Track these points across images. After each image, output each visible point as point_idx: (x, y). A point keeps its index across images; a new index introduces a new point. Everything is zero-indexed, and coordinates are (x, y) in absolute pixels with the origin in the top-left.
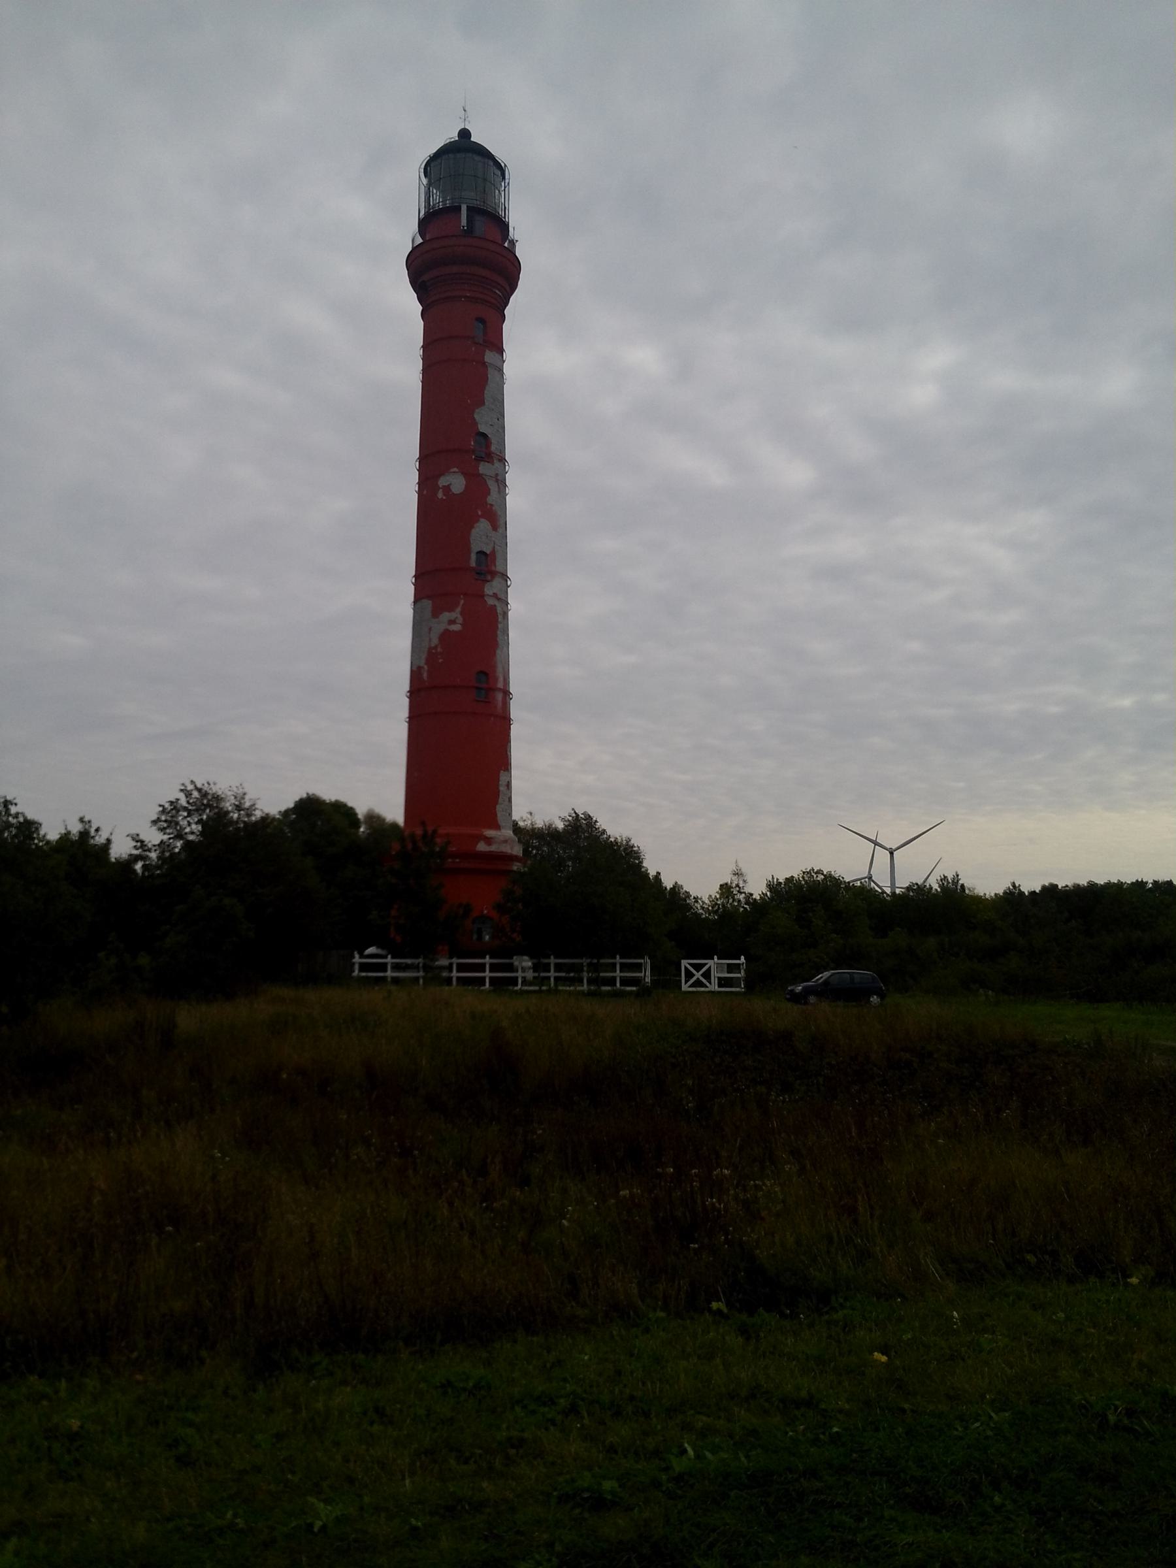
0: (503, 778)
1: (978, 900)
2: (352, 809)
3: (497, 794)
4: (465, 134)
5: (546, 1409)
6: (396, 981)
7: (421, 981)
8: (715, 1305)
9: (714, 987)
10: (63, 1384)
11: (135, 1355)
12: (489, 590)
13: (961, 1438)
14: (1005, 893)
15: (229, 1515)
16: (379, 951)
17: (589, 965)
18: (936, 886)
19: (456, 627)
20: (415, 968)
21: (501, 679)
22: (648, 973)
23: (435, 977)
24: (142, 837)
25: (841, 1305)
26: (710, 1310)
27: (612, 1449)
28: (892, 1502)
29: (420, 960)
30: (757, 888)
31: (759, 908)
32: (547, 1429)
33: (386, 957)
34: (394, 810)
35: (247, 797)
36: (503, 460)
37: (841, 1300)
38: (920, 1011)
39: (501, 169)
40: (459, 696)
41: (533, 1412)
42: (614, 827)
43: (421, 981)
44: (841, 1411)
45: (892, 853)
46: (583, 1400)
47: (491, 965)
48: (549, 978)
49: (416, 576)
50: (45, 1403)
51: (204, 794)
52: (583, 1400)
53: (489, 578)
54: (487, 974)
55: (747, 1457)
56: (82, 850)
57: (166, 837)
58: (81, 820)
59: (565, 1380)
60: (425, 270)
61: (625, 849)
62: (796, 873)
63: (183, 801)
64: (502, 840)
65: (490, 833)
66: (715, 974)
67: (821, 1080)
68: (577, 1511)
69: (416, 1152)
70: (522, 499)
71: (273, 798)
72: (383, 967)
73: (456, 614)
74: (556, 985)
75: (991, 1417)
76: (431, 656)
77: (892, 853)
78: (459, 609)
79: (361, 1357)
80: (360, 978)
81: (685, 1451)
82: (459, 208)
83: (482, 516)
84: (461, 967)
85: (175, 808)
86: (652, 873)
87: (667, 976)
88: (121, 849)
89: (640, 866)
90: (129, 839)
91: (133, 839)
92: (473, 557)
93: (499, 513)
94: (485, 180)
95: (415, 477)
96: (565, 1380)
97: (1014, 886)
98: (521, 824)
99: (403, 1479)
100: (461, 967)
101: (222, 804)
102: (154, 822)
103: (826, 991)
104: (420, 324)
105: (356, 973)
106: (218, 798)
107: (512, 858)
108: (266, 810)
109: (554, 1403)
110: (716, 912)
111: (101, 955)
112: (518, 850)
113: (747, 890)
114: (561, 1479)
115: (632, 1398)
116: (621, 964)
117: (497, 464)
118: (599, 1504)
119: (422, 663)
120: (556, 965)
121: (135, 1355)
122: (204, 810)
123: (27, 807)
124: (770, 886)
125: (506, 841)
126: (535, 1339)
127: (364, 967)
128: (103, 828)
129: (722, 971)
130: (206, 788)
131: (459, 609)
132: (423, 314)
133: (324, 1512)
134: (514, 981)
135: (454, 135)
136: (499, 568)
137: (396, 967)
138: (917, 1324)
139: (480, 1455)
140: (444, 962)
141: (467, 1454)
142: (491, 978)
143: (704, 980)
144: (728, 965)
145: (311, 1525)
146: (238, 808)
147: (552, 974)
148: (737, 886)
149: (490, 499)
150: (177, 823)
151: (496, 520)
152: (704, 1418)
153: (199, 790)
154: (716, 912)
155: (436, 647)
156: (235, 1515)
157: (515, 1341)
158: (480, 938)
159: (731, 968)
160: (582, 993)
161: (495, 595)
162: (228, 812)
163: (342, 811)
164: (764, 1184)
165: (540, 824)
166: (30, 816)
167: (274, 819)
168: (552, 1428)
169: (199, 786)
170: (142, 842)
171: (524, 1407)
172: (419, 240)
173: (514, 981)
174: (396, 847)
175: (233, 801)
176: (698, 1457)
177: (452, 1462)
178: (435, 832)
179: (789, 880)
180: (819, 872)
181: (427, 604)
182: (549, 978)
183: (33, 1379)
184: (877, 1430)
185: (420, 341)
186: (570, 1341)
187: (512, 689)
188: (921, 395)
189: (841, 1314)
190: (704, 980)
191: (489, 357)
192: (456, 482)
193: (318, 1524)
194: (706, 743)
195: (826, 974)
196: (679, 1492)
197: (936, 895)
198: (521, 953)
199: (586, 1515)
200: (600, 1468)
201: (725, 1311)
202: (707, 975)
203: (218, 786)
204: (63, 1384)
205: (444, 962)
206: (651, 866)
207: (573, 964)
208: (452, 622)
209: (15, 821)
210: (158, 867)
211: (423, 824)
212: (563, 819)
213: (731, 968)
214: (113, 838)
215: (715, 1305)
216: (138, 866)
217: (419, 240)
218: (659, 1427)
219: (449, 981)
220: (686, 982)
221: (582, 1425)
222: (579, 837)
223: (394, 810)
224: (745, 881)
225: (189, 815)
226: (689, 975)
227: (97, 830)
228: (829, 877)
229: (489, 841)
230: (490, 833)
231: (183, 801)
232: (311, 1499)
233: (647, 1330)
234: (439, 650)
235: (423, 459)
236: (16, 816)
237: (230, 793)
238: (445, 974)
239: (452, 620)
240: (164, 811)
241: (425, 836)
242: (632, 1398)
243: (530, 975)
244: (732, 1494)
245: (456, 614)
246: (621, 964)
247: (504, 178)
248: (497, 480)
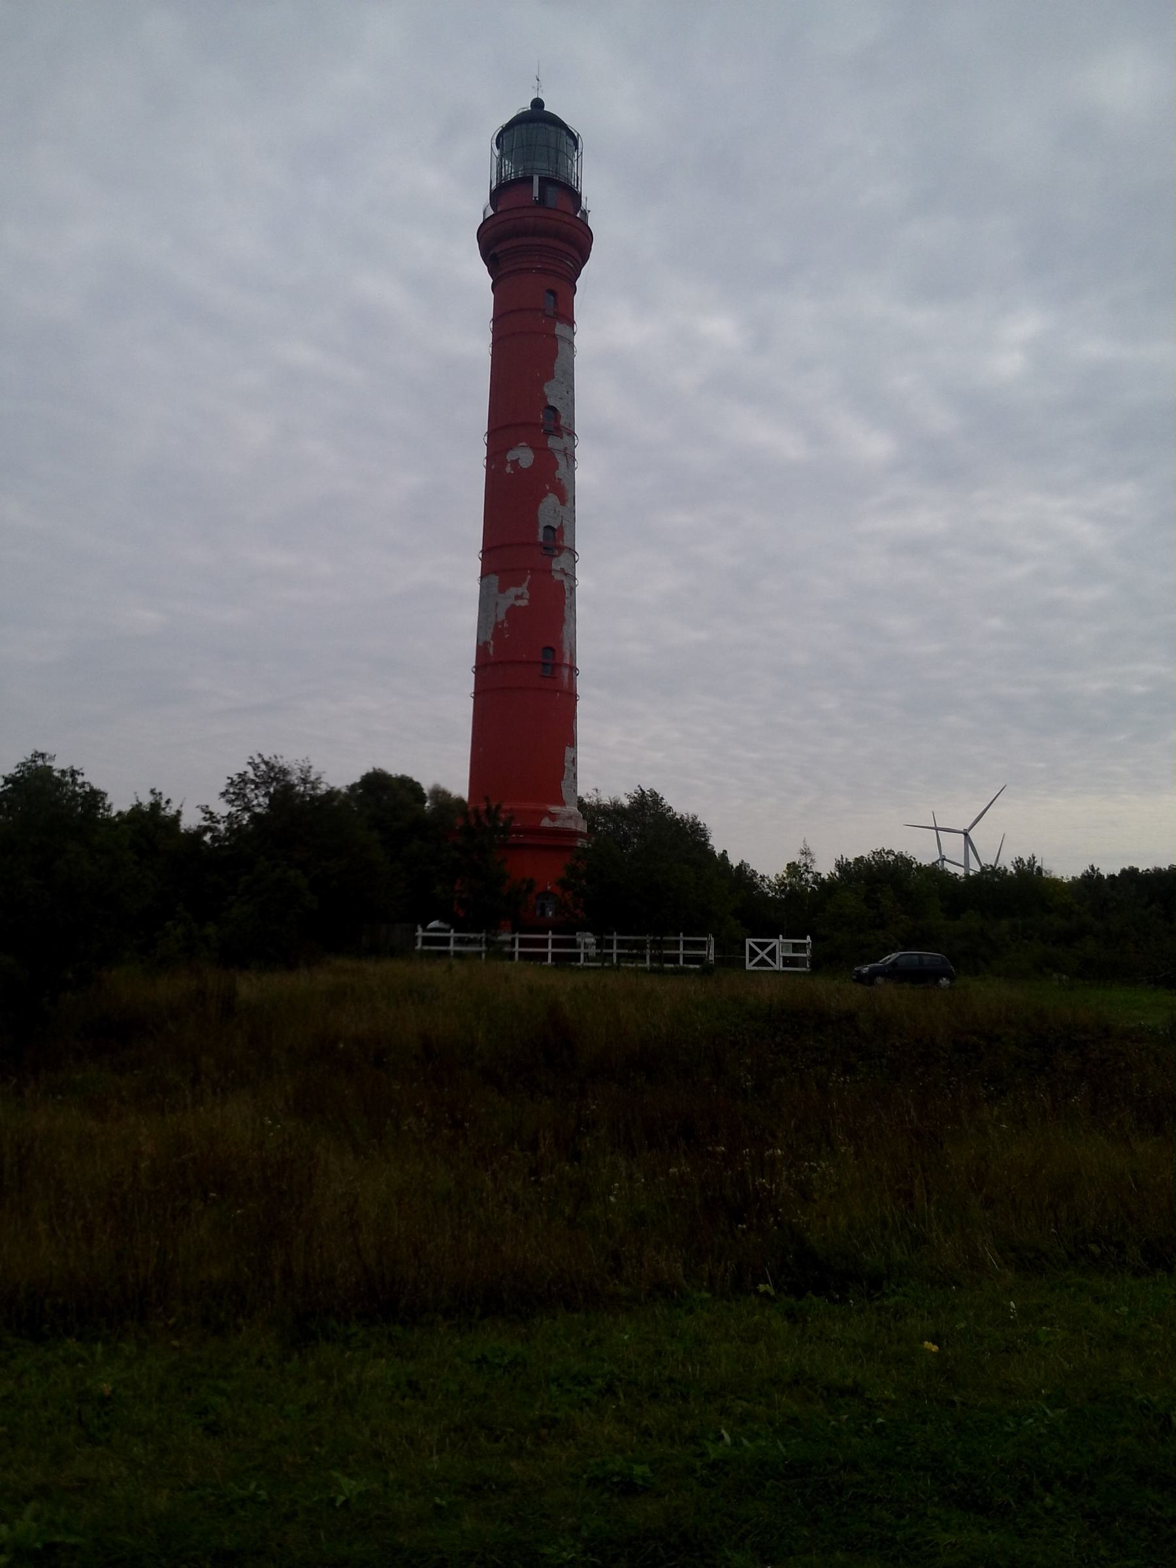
1: (1056, 883)
2: (418, 783)
3: (562, 769)
4: (538, 104)
5: (583, 1389)
6: (458, 955)
7: (483, 955)
8: (762, 1287)
9: (779, 966)
10: (99, 1347)
11: (172, 1321)
12: (556, 565)
13: (1013, 1434)
14: (1083, 876)
15: (252, 1486)
16: (442, 925)
17: (653, 942)
18: (1011, 869)
19: (523, 603)
20: (478, 942)
21: (568, 655)
22: (712, 951)
23: (498, 952)
24: (211, 809)
25: (893, 1291)
26: (757, 1292)
27: (646, 1432)
28: (936, 1499)
29: (483, 935)
30: (825, 868)
31: (827, 887)
32: (581, 1409)
33: (449, 931)
34: (459, 786)
35: (313, 770)
36: (572, 434)
37: (893, 1286)
38: (988, 994)
39: (574, 139)
40: (525, 671)
41: (569, 1391)
42: (680, 804)
43: (483, 955)
44: (887, 1401)
45: (966, 835)
46: (620, 1380)
48: (611, 954)
49: (482, 551)
50: (80, 1365)
52: (620, 1380)
53: (556, 552)
55: (785, 1445)
56: (151, 823)
57: (234, 809)
58: (152, 792)
59: (603, 1360)
60: (498, 242)
61: (691, 827)
62: (865, 852)
63: (251, 775)
64: (567, 817)
66: (780, 954)
67: (884, 1061)
68: (606, 1495)
69: (467, 1125)
70: (590, 473)
71: (339, 773)
72: (446, 941)
73: (523, 590)
74: (618, 961)
75: (1045, 1414)
76: (498, 632)
77: (966, 835)
78: (525, 585)
79: (398, 1329)
80: (422, 952)
81: (721, 1437)
82: (531, 180)
84: (524, 943)
85: (243, 780)
86: (718, 851)
87: (731, 954)
88: (191, 820)
89: (705, 844)
90: (199, 810)
91: (203, 811)
92: (541, 531)
93: (565, 482)
94: (558, 151)
95: (484, 452)
96: (603, 1360)
97: (1093, 869)
98: (587, 800)
99: (431, 1455)
100: (524, 943)
101: (288, 778)
102: (223, 794)
103: (895, 973)
105: (419, 947)
106: (284, 772)
107: (575, 834)
108: (332, 785)
109: (590, 1383)
110: (783, 892)
111: (169, 924)
112: (582, 826)
113: (815, 869)
114: (592, 1461)
115: (671, 1380)
116: (685, 942)
117: (566, 438)
118: (629, 1488)
119: (489, 637)
120: (619, 941)
121: (172, 1321)
122: (271, 783)
123: (94, 777)
124: (839, 866)
125: (570, 817)
126: (576, 1316)
127: (427, 941)
128: (173, 799)
129: (787, 951)
130: (273, 761)
131: (525, 585)
132: (494, 287)
133: (349, 1487)
134: (576, 957)
135: (527, 105)
136: (566, 543)
137: (459, 941)
138: (971, 1314)
139: (512, 1434)
140: (506, 937)
141: (498, 1432)
142: (553, 954)
143: (769, 960)
144: (794, 945)
145: (333, 1500)
146: (304, 781)
147: (615, 950)
148: (805, 865)
149: (560, 473)
150: (245, 796)
151: (564, 494)
152: (745, 1404)
153: (267, 763)
154: (783, 892)
155: (503, 622)
156: (258, 1487)
157: (555, 1318)
158: (543, 913)
159: (796, 948)
160: (644, 970)
161: (562, 570)
162: (294, 786)
163: (408, 786)
164: (819, 1166)
165: (606, 800)
166: (96, 786)
167: (339, 792)
168: (587, 1409)
169: (266, 759)
170: (211, 813)
171: (560, 1385)
172: (491, 212)
173: (576, 957)
174: (459, 822)
175: (299, 774)
176: (736, 1443)
177: (482, 1440)
178: (498, 807)
179: (859, 860)
180: (890, 852)
181: (494, 579)
182: (611, 954)
183: (71, 1342)
184: (924, 1422)
186: (611, 1319)
187: (579, 665)
188: (1008, 365)
189: (893, 1300)
190: (769, 960)
191: (560, 329)
192: (525, 457)
193: (341, 1499)
194: (773, 720)
195: (894, 956)
196: (713, 1480)
197: (1012, 877)
198: (585, 928)
199: (615, 1500)
200: (633, 1451)
201: (773, 1293)
202: (772, 954)
203: (285, 760)
204: (99, 1347)
205: (506, 937)
206: (717, 844)
207: (635, 935)
208: (517, 597)
209: (80, 791)
210: (226, 839)
211: (487, 799)
212: (629, 796)
213: (796, 948)
214: (183, 810)
215: (762, 1287)
216: (207, 838)
217: (491, 212)
218: (697, 1412)
219: (511, 956)
220: (751, 961)
221: (618, 1406)
222: (644, 814)
223: (459, 786)
224: (812, 860)
225: (257, 788)
226: (754, 953)
227: (168, 802)
228: (900, 858)
229: (553, 817)
231: (251, 775)
232: (335, 1474)
233: (691, 1311)
234: (506, 625)
235: (491, 434)
236: (83, 785)
237: (296, 767)
238: (507, 949)
239: (519, 595)
240: (232, 784)
241: (488, 811)
242: (671, 1380)
243: (593, 951)
244: (768, 1484)
245: (523, 590)
246: (685, 942)
247: (577, 148)
248: (566, 455)
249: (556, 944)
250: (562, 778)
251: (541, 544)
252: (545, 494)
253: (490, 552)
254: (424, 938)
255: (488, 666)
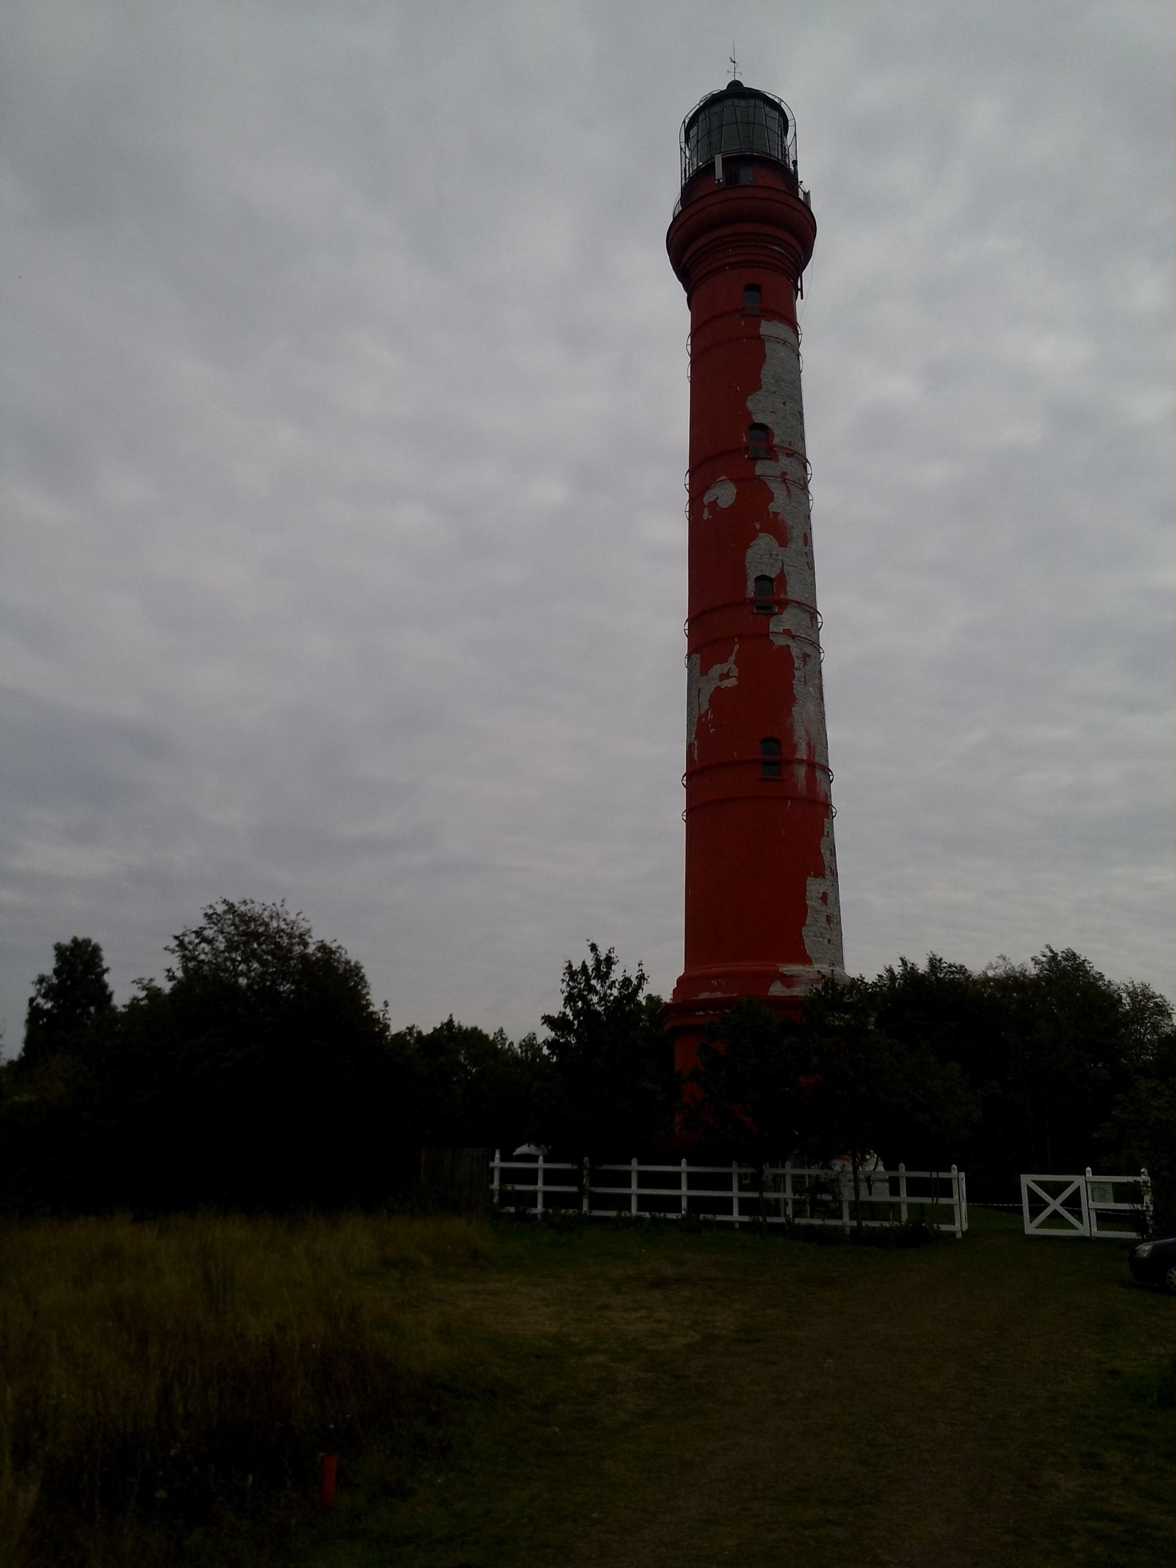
0: (814, 887)
9: (1087, 1228)
19: (731, 682)
47: (690, 1175)
51: (246, 919)
54: (684, 1191)
65: (788, 969)
66: (1089, 1205)
73: (730, 665)
78: (733, 658)
83: (762, 530)
92: (751, 586)
104: (687, 315)
105: (496, 1185)
129: (1103, 1199)
131: (733, 658)
144: (1115, 1184)
149: (780, 502)
161: (787, 632)
181: (697, 657)
185: (688, 329)
202: (1073, 1203)
208: (724, 677)
213: (1121, 1193)
226: (1037, 1205)
229: (788, 981)
230: (788, 969)
245: (730, 665)
248: (784, 480)
249: (695, 1181)
250: (804, 924)
251: (752, 601)
252: (754, 535)
253: (697, 620)
254: (503, 1171)
255: (702, 774)
